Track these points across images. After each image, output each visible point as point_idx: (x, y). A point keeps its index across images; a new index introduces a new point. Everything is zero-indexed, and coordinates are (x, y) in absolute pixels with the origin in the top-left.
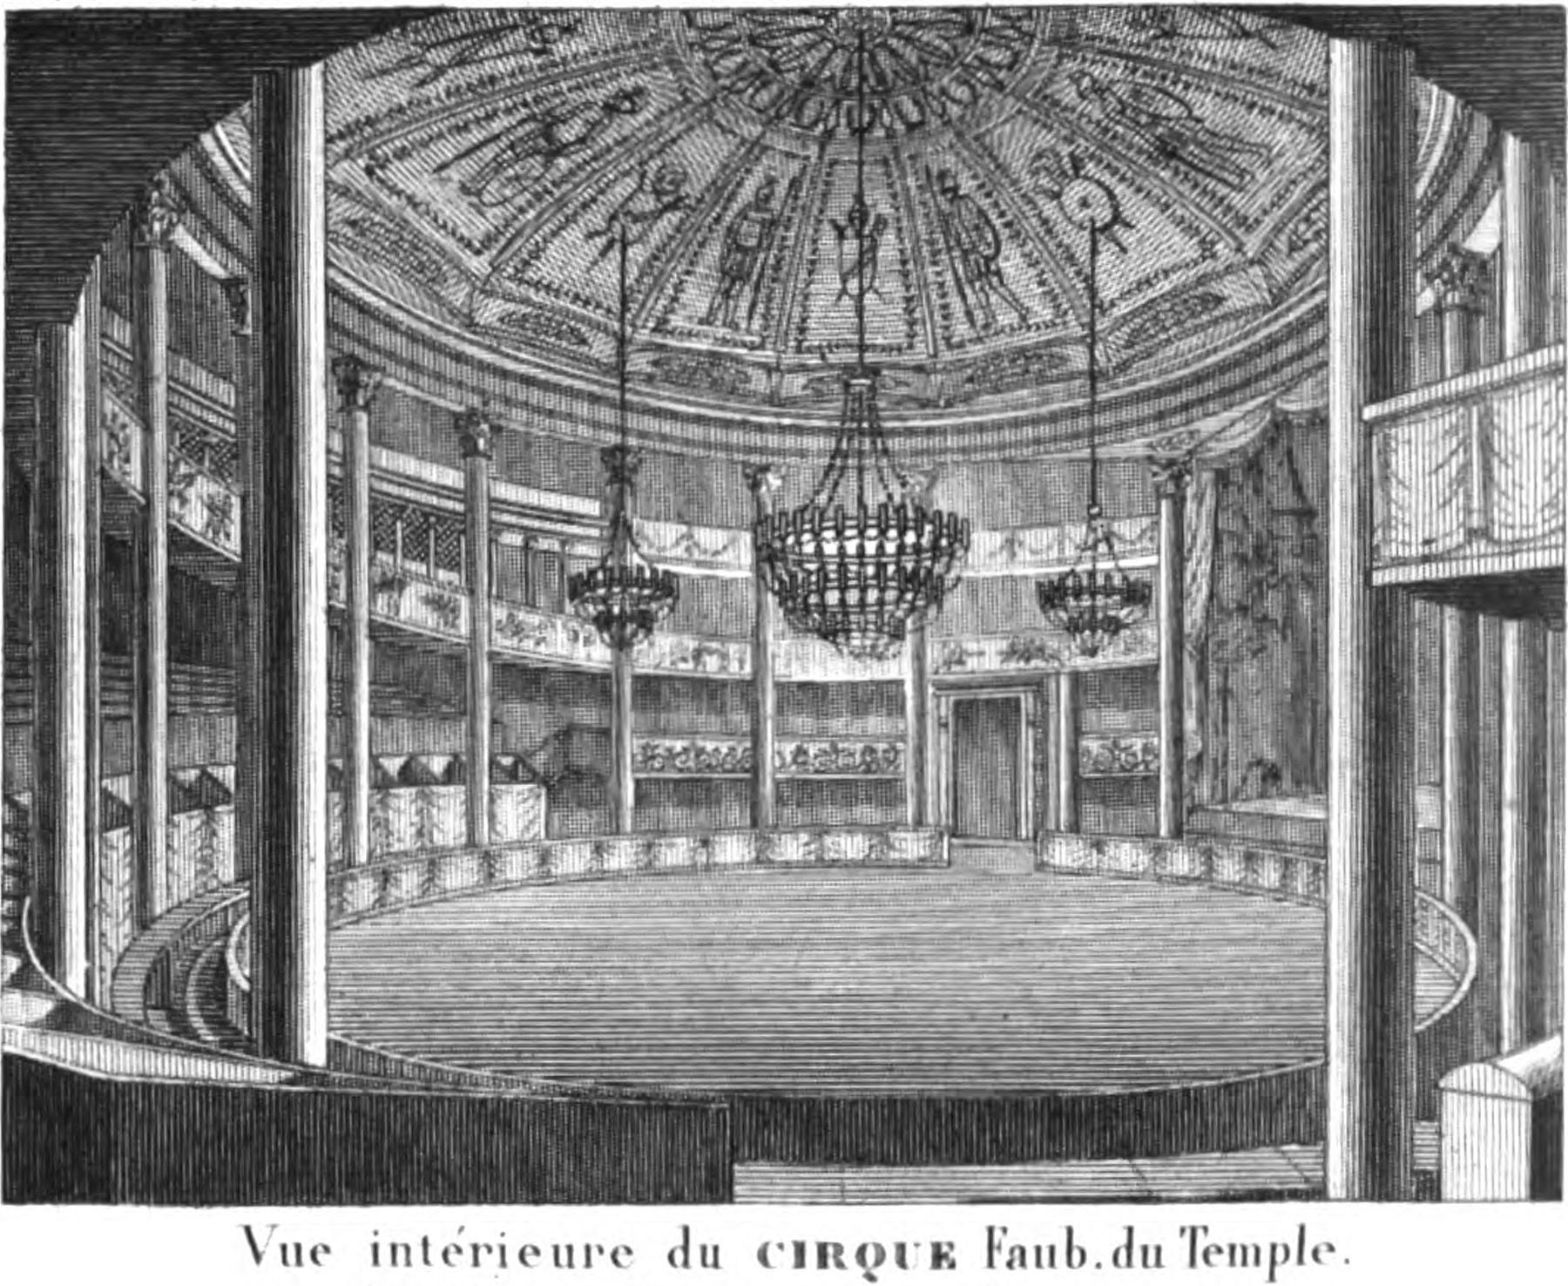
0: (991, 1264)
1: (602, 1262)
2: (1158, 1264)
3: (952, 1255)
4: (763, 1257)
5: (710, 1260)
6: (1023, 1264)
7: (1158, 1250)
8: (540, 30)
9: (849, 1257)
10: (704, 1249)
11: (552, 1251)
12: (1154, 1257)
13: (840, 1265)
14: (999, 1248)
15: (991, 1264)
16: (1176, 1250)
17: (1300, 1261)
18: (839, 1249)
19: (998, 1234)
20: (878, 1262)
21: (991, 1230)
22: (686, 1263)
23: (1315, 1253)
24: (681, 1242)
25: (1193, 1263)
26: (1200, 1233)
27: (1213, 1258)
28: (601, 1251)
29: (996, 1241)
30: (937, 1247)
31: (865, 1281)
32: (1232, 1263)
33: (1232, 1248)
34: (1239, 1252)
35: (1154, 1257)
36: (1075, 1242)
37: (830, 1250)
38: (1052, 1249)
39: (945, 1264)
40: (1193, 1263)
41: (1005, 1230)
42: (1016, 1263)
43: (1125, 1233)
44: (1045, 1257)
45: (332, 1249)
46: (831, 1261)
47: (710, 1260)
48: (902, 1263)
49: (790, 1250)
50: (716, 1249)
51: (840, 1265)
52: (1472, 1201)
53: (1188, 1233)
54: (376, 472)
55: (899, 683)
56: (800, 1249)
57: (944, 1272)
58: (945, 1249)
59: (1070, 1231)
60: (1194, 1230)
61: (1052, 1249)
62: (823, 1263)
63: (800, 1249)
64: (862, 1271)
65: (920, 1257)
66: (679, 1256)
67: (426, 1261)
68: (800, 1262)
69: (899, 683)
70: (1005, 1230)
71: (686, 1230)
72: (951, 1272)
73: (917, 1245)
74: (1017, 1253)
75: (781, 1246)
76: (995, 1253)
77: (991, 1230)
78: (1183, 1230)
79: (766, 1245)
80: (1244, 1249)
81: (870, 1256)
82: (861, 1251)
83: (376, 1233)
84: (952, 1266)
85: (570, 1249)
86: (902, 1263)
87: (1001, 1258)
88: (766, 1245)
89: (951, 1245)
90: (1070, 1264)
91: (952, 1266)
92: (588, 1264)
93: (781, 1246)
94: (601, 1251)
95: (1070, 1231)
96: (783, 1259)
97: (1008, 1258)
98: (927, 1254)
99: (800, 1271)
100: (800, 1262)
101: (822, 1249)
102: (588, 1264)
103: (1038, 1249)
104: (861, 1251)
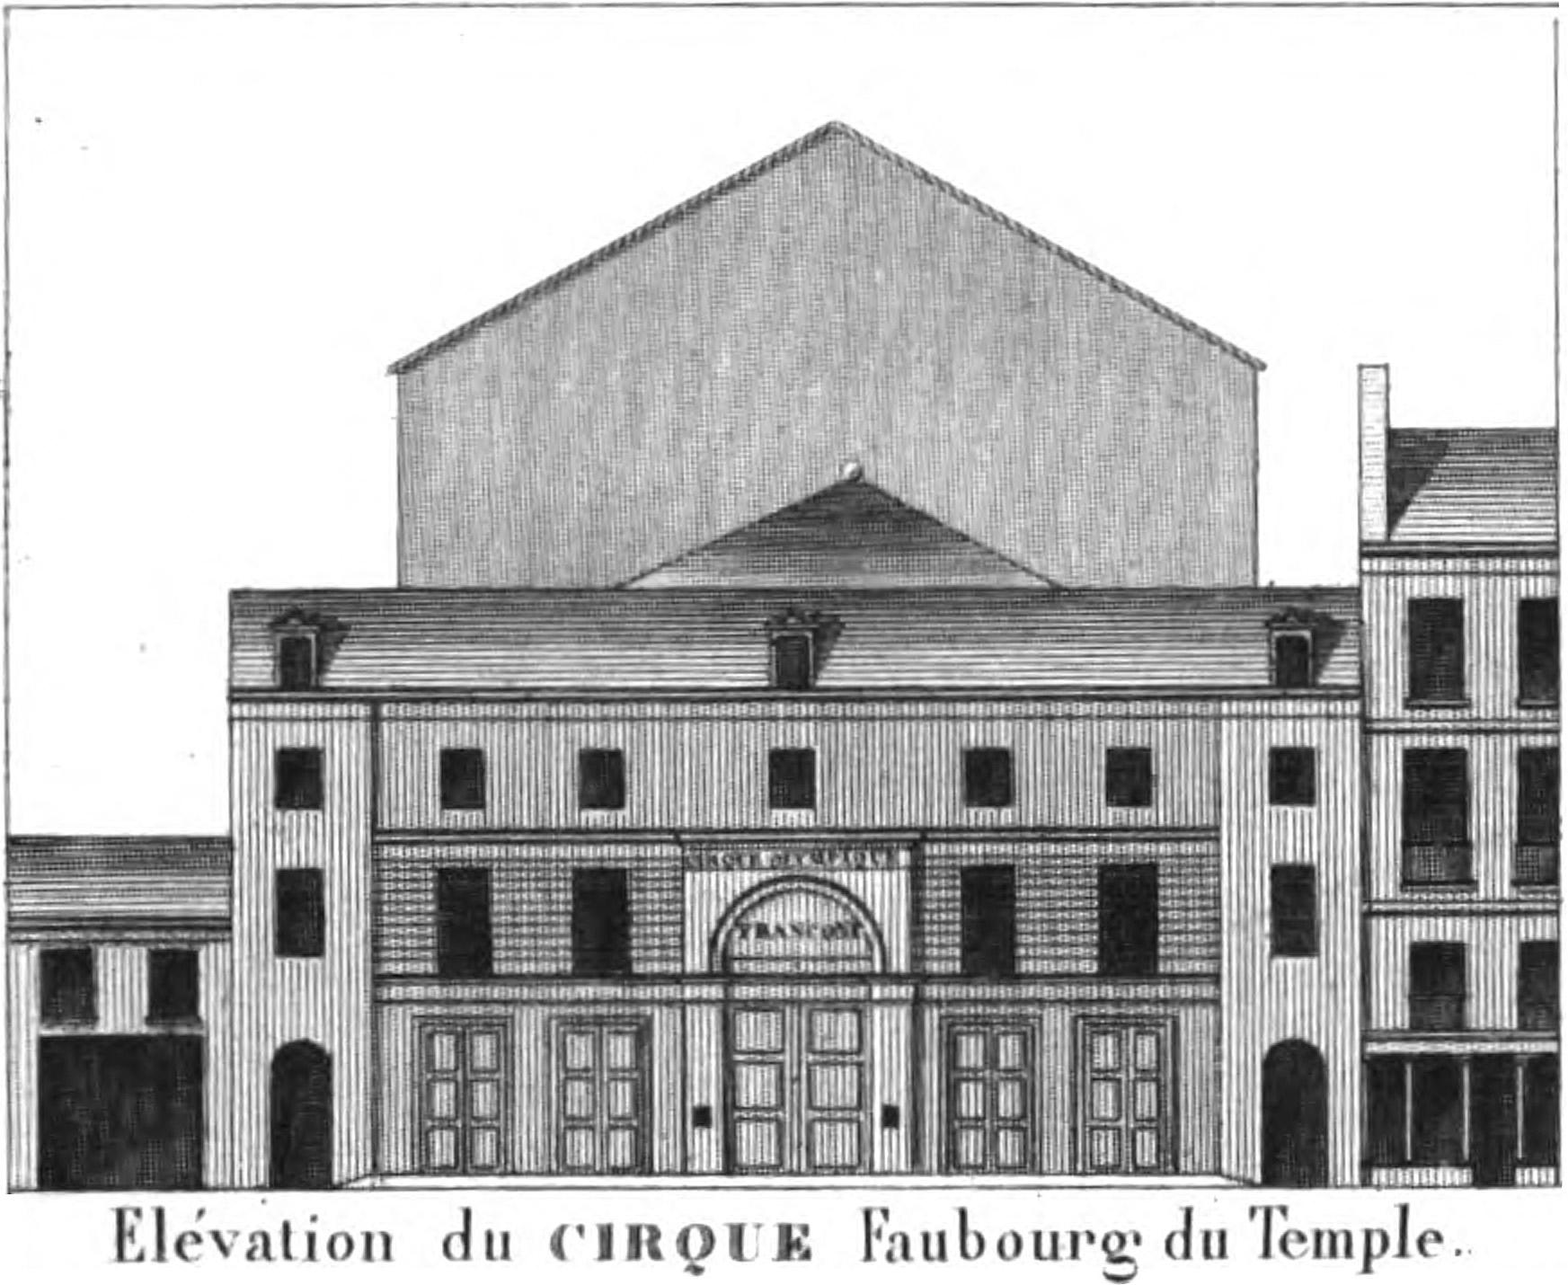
0: (868, 1256)
2: (387, 1256)
3: (806, 1242)
4: (558, 1248)
5: (1215, 1250)
6: (906, 1255)
9: (667, 1244)
10: (1207, 1236)
11: (921, 1239)
13: (655, 1254)
14: (132, 1234)
15: (868, 1256)
16: (1245, 1238)
17: (1403, 1253)
18: (655, 1233)
19: (877, 1219)
20: (706, 1252)
21: (868, 1214)
24: (1181, 1226)
25: (1267, 1253)
26: (1276, 1215)
27: (1293, 1247)
28: (1091, 1238)
30: (786, 1230)
31: (689, 1275)
32: (1318, 1253)
33: (1318, 1235)
35: (500, 1247)
36: (971, 1226)
37: (645, 1235)
38: (942, 1236)
39: (795, 1254)
40: (1267, 1253)
41: (885, 1212)
42: (258, 1253)
43: (1181, 1216)
45: (1444, 1234)
46: (644, 1250)
47: (1215, 1250)
48: (737, 1250)
51: (655, 1254)
53: (1260, 1215)
54: (16, 924)
56: (606, 1234)
57: (795, 1265)
58: (796, 1233)
60: (1268, 1212)
61: (942, 1236)
62: (635, 1254)
63: (606, 1234)
64: (686, 1263)
65: (763, 1243)
68: (606, 1254)
70: (885, 1212)
71: (467, 1214)
72: (805, 1263)
74: (259, 1241)
75: (581, 1229)
77: (868, 1214)
78: (1253, 1211)
79: (562, 1229)
80: (1333, 1236)
82: (683, 1239)
83: (314, 1219)
84: (807, 1255)
85: (1055, 1236)
86: (737, 1250)
87: (880, 1248)
88: (562, 1229)
89: (805, 1230)
90: (964, 1254)
91: (807, 1255)
92: (1075, 1255)
94: (1091, 1238)
96: (583, 1248)
98: (770, 1241)
99: (606, 1263)
100: (606, 1254)
101: (635, 1232)
102: (1075, 1255)
103: (926, 1237)
104: (683, 1239)
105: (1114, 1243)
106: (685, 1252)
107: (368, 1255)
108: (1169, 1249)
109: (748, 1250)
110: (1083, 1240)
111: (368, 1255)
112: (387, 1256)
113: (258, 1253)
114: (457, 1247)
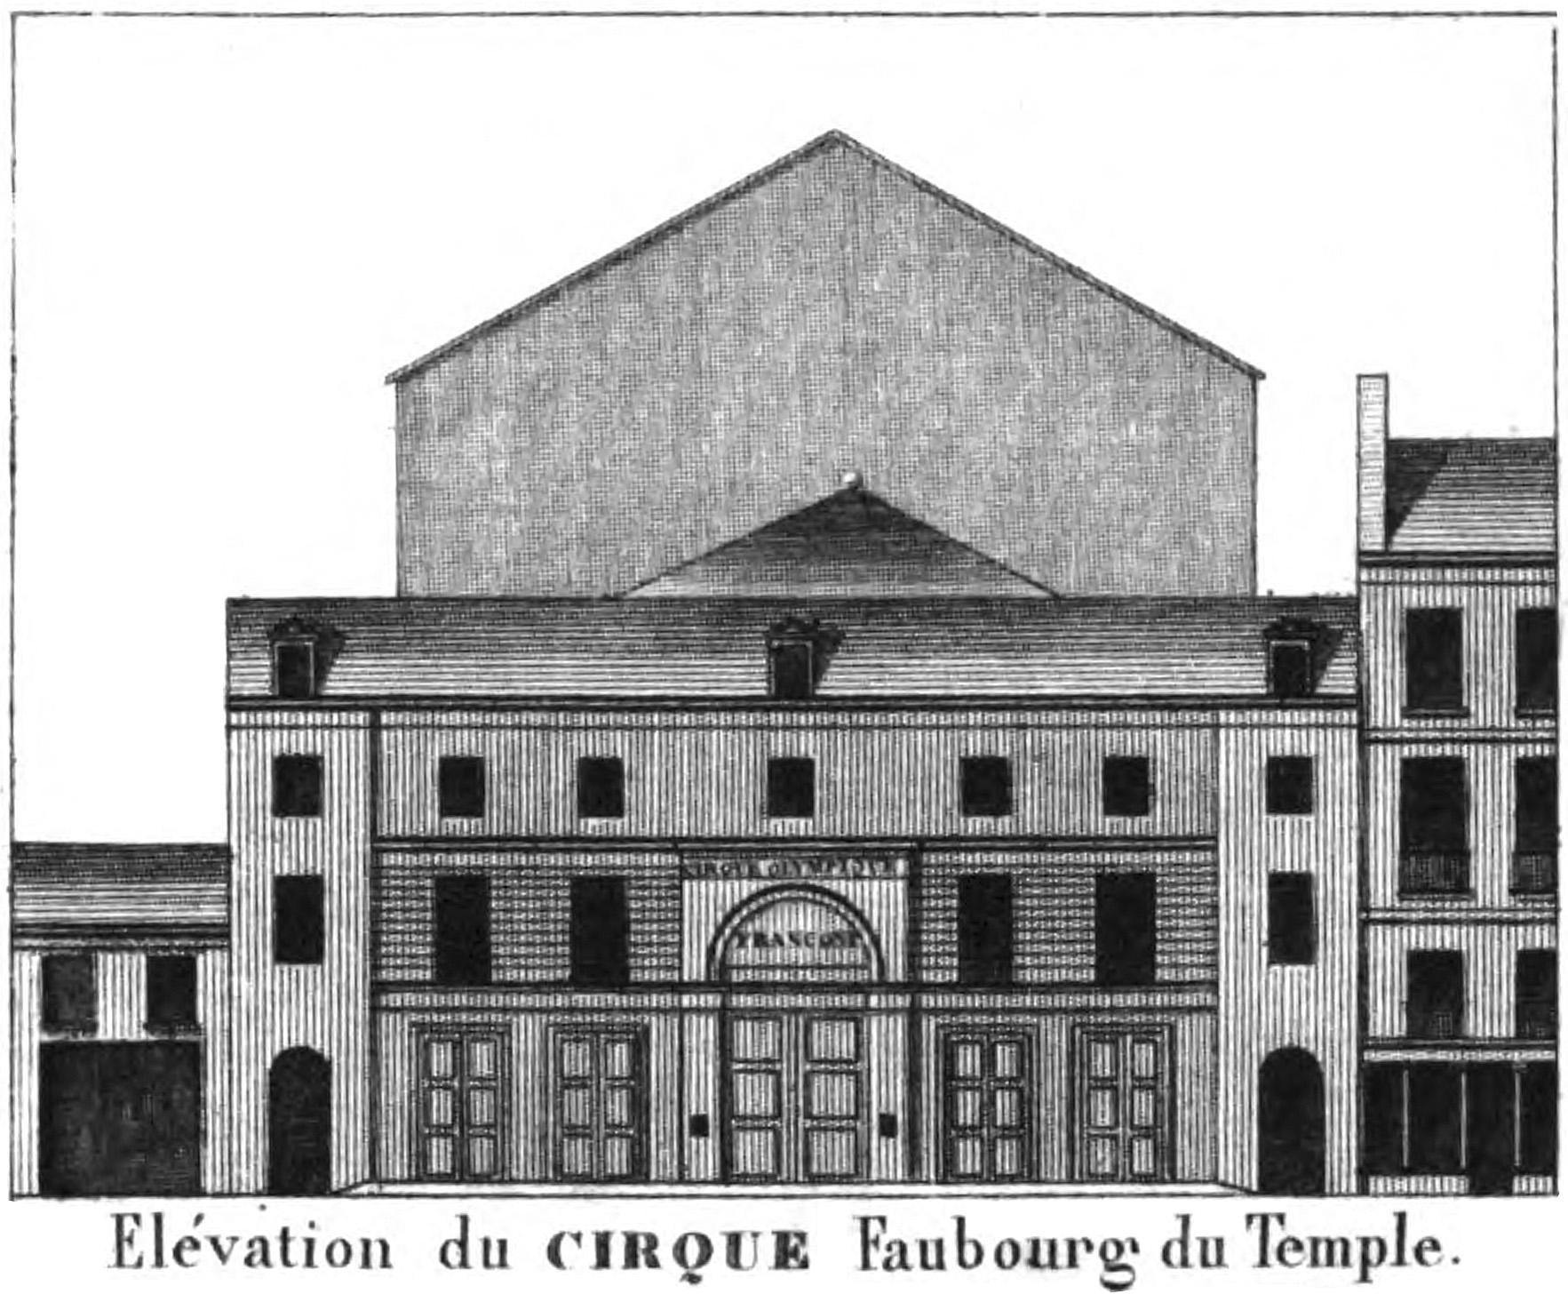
1: (1091, 1263)
2: (385, 1263)
7: (503, 1244)
8: (533, 512)
9: (664, 1253)
12: (1214, 1254)
13: (653, 1263)
15: (866, 1265)
16: (1242, 1246)
18: (652, 1241)
19: (874, 1227)
20: (705, 1258)
22: (464, 1264)
23: (1419, 1252)
25: (1263, 1262)
27: (1291, 1256)
28: (1089, 1247)
29: (872, 1235)
30: (782, 1237)
32: (1315, 1262)
33: (1315, 1242)
34: (1322, 1248)
35: (1214, 1254)
36: (968, 1234)
37: (642, 1243)
40: (1263, 1262)
42: (257, 1259)
43: (458, 1222)
44: (932, 1257)
46: (642, 1259)
48: (734, 1261)
49: (589, 1243)
50: (1220, 1242)
52: (239, 1195)
53: (1257, 1222)
55: (1406, 763)
56: (603, 1241)
57: (792, 1276)
58: (793, 1241)
59: (961, 1221)
62: (631, 1262)
63: (603, 1241)
64: (682, 1271)
66: (456, 1251)
67: (286, 1263)
68: (603, 1261)
69: (1406, 763)
72: (803, 1272)
73: (755, 1235)
76: (872, 1249)
78: (1250, 1218)
79: (558, 1239)
81: (693, 1251)
84: (804, 1264)
86: (734, 1261)
87: (877, 1257)
89: (802, 1237)
91: (804, 1264)
93: (578, 1237)
94: (1089, 1247)
95: (961, 1221)
96: (580, 1256)
97: (247, 1252)
98: (768, 1247)
100: (603, 1261)
101: (632, 1240)
105: (1112, 1252)
106: (681, 1258)
107: (366, 1263)
108: (444, 1259)
109: (746, 1257)
110: (1081, 1248)
111: (366, 1263)
112: (385, 1263)
113: (257, 1259)
114: (454, 1254)
